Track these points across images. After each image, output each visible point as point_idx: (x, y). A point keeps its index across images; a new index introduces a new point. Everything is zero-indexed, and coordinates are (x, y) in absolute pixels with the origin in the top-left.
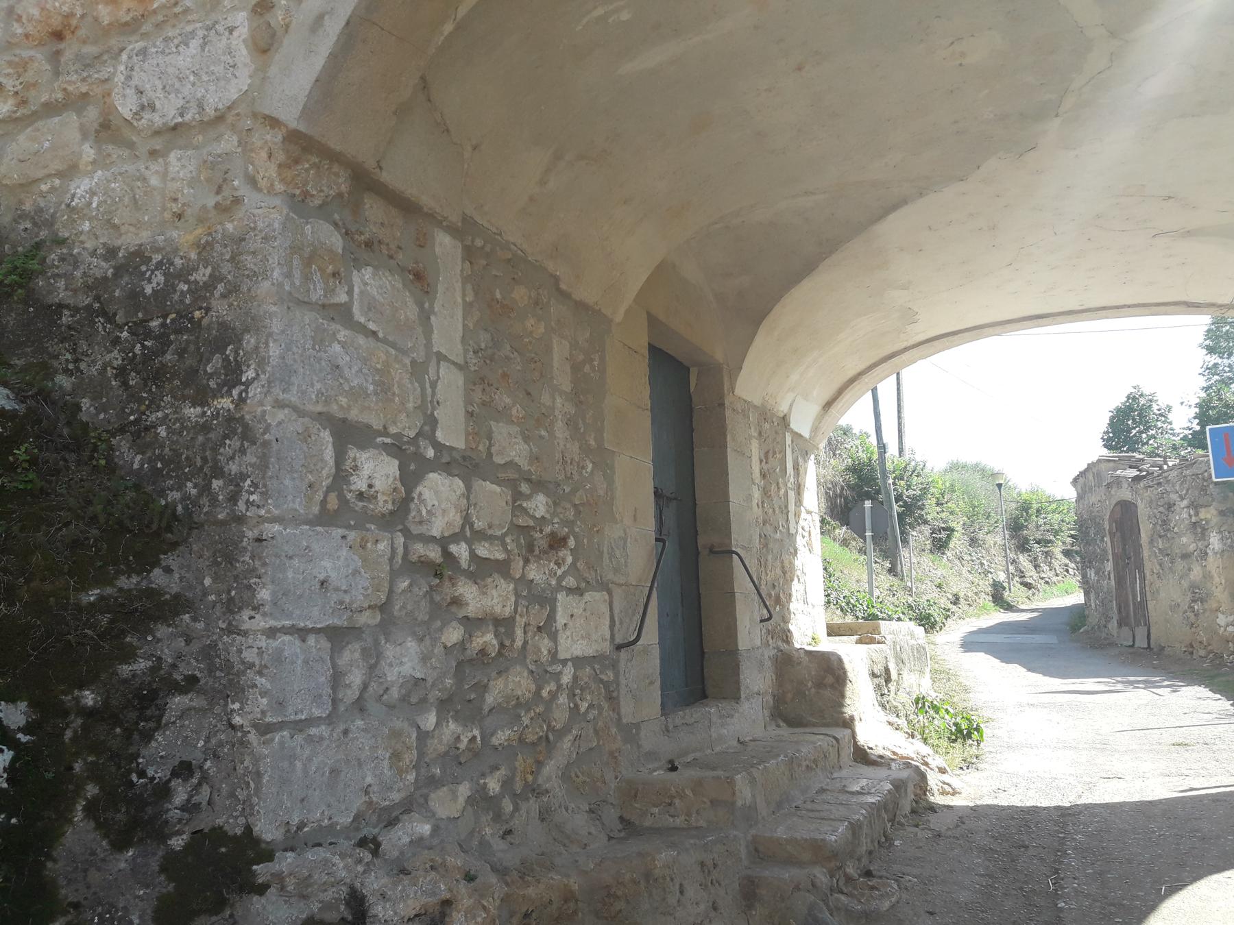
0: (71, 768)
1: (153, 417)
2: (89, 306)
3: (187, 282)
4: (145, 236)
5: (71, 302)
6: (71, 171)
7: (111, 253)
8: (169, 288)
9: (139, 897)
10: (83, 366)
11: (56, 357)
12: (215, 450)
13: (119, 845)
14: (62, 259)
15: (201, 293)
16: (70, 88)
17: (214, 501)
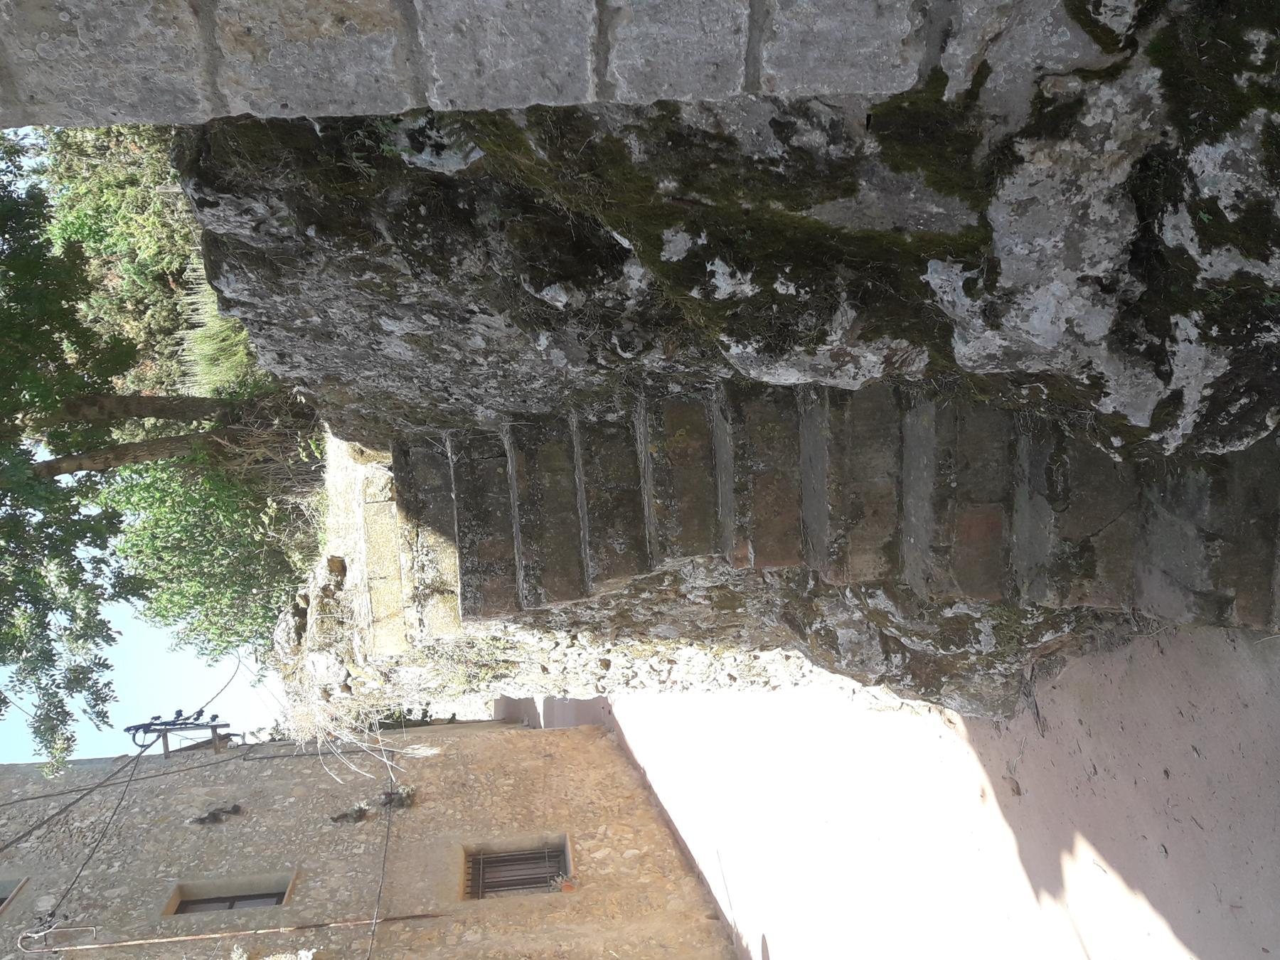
0: (747, 212)
9: (915, 200)
13: (851, 190)
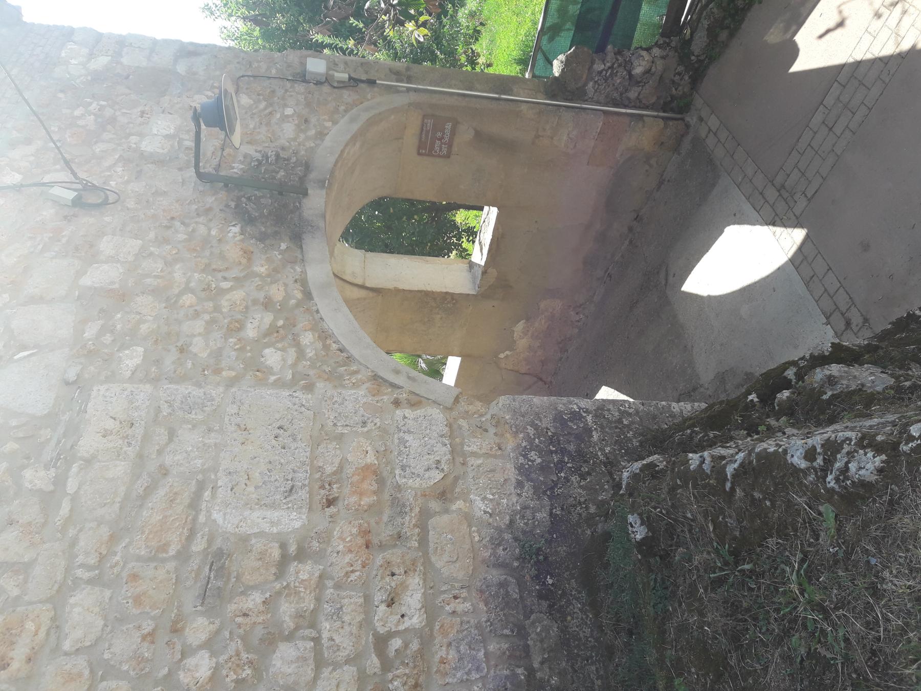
1: (601, 457)
2: (550, 498)
3: (534, 439)
4: (510, 466)
5: (548, 508)
6: (468, 518)
7: (520, 484)
8: (537, 449)
10: (582, 500)
11: (580, 514)
12: (611, 422)
14: (523, 517)
15: (539, 432)
16: (414, 521)
17: (632, 423)
